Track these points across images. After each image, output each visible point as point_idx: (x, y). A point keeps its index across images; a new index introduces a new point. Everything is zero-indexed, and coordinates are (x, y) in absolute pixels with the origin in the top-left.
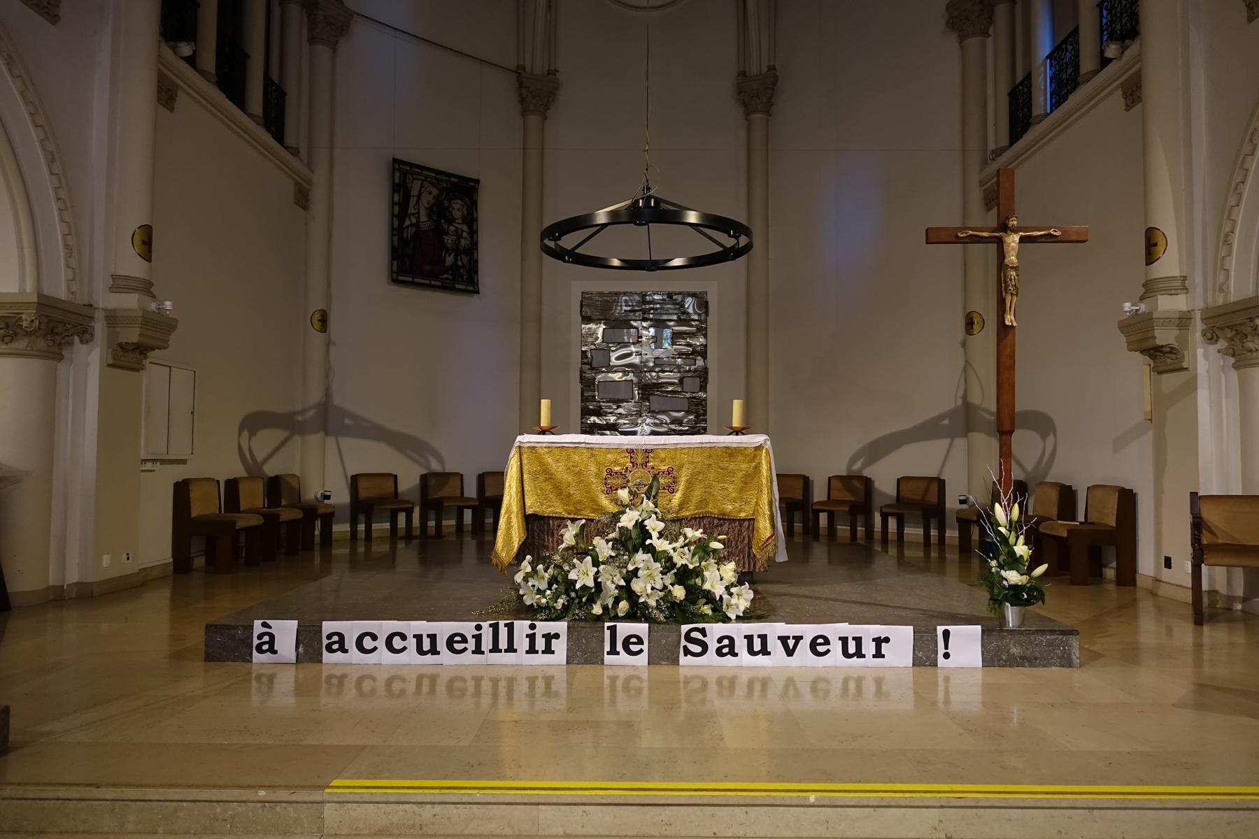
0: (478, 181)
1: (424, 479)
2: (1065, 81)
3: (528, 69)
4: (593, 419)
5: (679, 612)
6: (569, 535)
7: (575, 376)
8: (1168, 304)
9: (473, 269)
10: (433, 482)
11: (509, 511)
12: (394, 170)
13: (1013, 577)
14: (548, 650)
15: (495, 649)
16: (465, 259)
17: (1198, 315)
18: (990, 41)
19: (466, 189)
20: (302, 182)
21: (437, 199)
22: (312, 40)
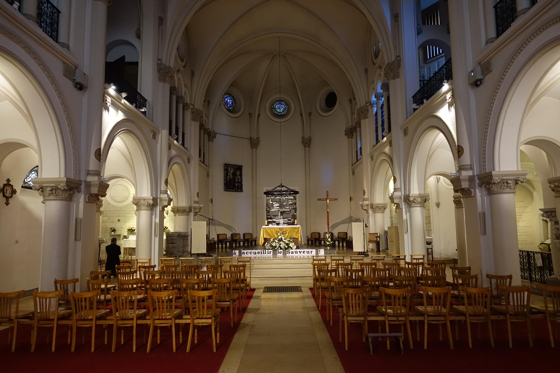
0: (242, 166)
1: (232, 235)
2: (506, 18)
4: (270, 220)
5: (286, 249)
6: (272, 240)
7: (265, 210)
8: (366, 203)
9: (242, 187)
10: (234, 235)
11: (261, 237)
13: (328, 243)
14: (270, 253)
15: (263, 253)
16: (240, 184)
17: (369, 205)
18: (353, 139)
19: (239, 168)
20: (68, 63)
22: (209, 141)
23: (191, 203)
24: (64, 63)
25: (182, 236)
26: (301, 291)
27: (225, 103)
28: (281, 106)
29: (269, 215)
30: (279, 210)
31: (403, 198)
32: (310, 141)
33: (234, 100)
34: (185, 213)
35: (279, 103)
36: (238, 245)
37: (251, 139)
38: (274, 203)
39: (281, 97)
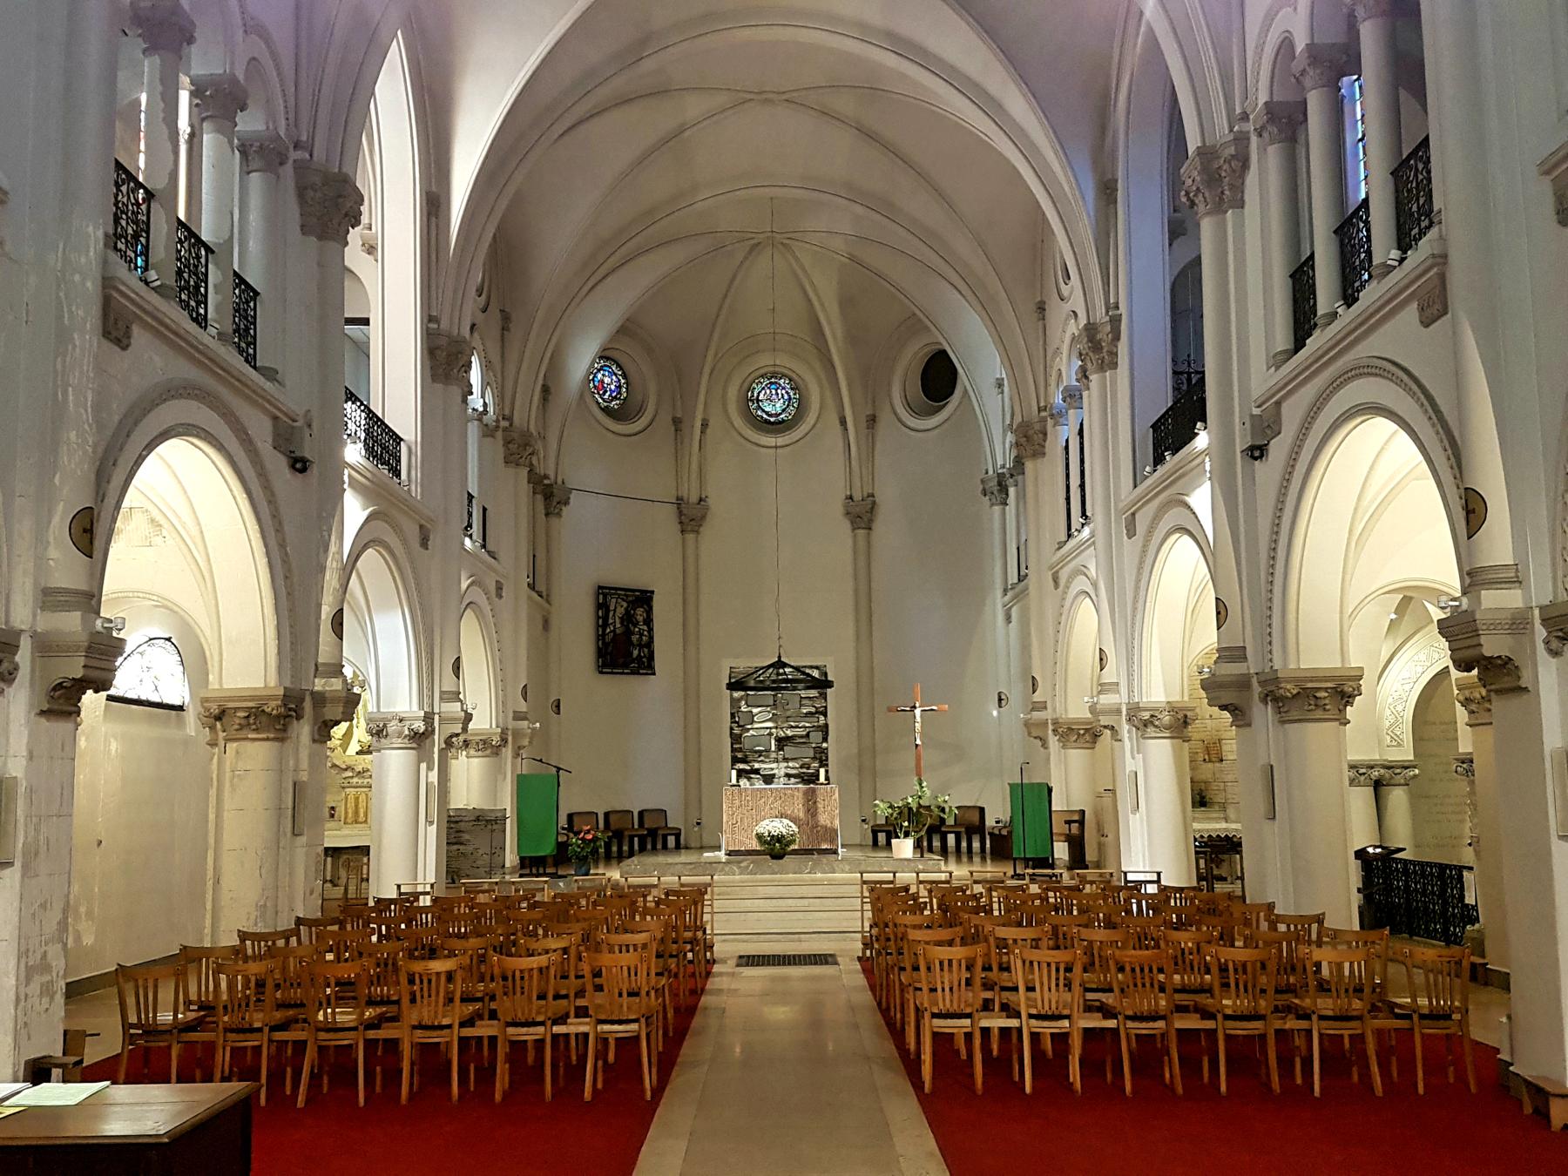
0: (653, 592)
3: (685, 498)
4: (742, 766)
8: (1495, 600)
9: (651, 657)
12: (599, 594)
16: (646, 650)
18: (1007, 507)
19: (644, 599)
21: (626, 609)
22: (547, 515)
23: (506, 717)
24: (275, 418)
25: (487, 821)
26: (836, 963)
27: (595, 387)
28: (777, 394)
29: (740, 750)
30: (770, 734)
31: (1124, 712)
32: (872, 508)
33: (625, 376)
34: (488, 752)
35: (771, 383)
36: (625, 848)
37: (680, 502)
38: (755, 711)
39: (778, 362)
